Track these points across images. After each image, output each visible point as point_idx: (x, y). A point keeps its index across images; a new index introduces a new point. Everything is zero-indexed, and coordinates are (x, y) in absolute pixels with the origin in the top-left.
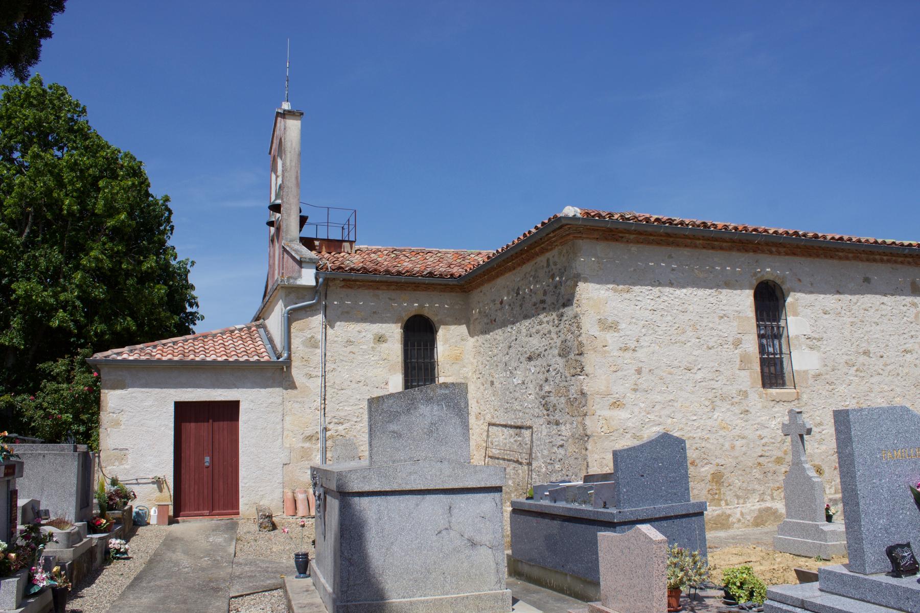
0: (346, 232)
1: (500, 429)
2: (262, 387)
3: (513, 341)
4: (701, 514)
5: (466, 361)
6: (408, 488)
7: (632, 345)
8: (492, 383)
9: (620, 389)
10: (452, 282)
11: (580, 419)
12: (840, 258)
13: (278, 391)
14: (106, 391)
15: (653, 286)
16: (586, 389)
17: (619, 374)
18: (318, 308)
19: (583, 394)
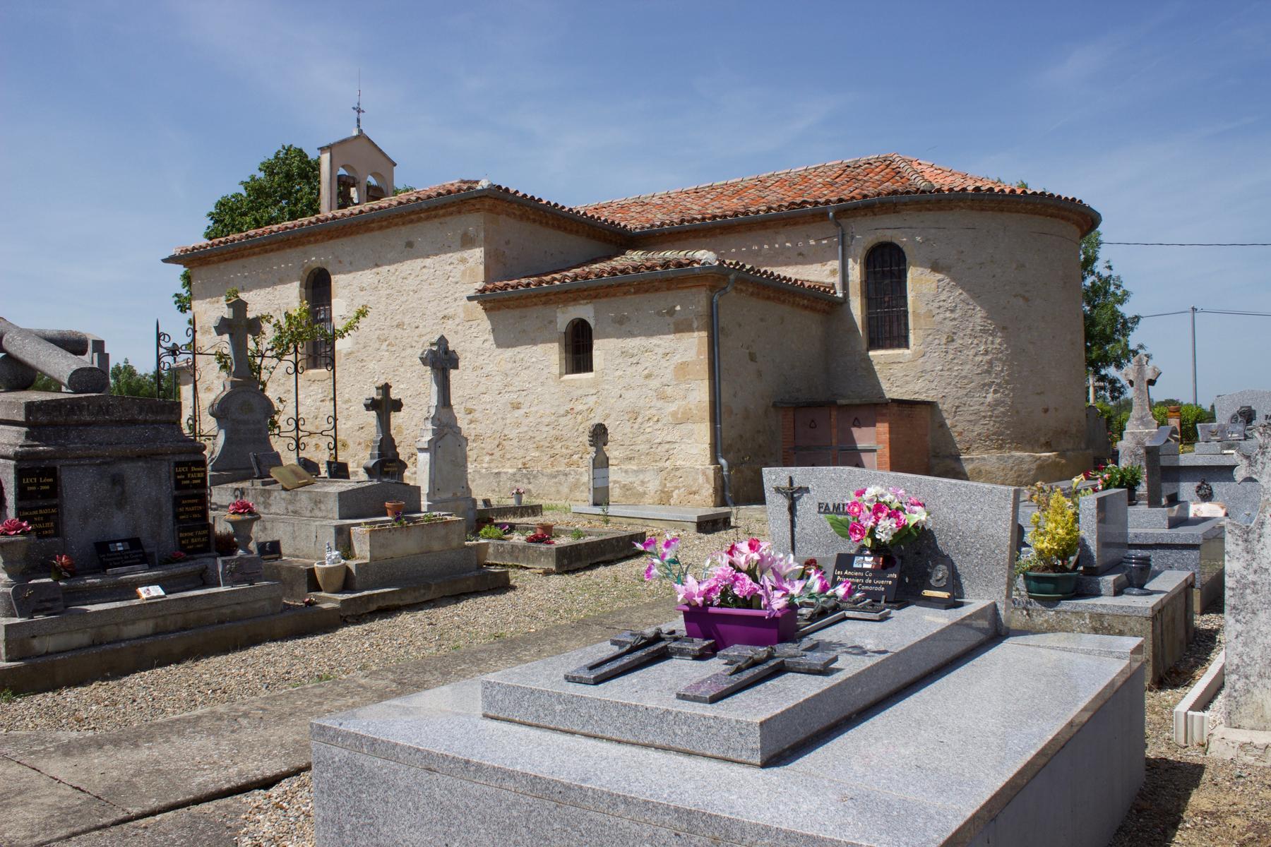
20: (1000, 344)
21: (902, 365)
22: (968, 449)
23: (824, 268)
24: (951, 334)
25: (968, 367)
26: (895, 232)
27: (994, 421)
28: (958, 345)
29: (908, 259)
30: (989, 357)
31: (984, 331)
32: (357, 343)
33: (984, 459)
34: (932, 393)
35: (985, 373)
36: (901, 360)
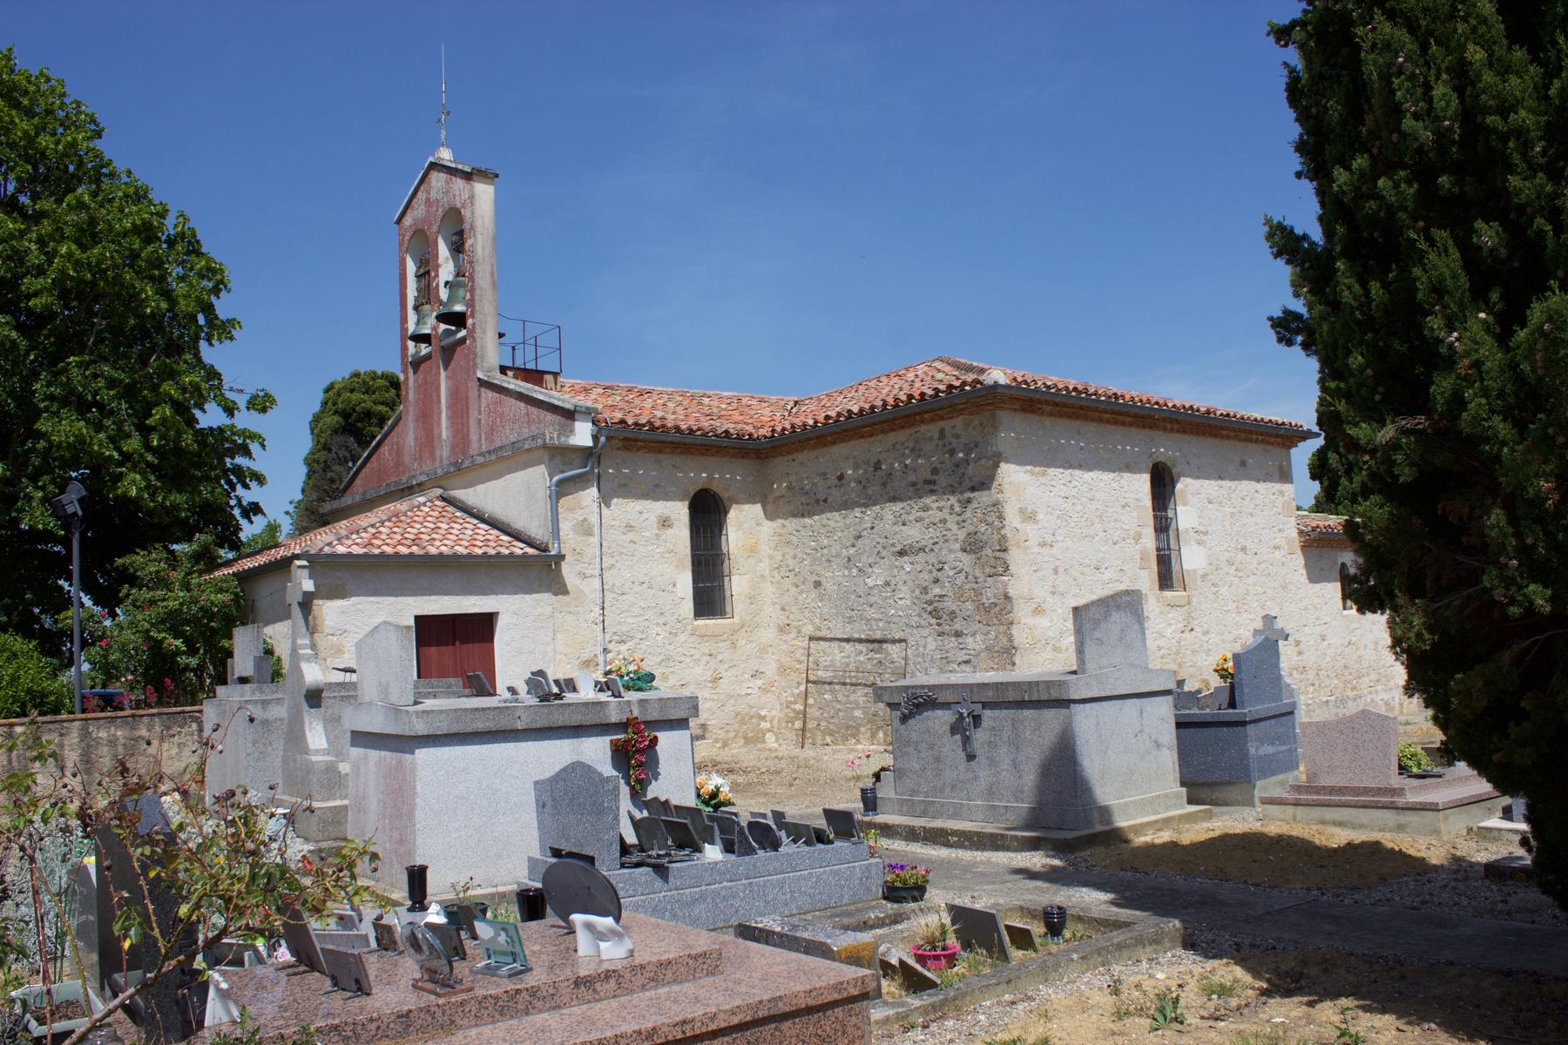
0: (519, 353)
1: (835, 644)
2: (526, 593)
3: (865, 529)
4: (1291, 713)
5: (762, 553)
6: (1116, 693)
7: (1049, 539)
8: (817, 584)
9: (1041, 592)
10: (677, 438)
11: (1002, 628)
12: (1222, 437)
13: (546, 596)
14: (321, 602)
15: (1065, 468)
16: (1011, 592)
17: (1040, 574)
18: (590, 477)
19: (1007, 597)
32: (1211, 564)
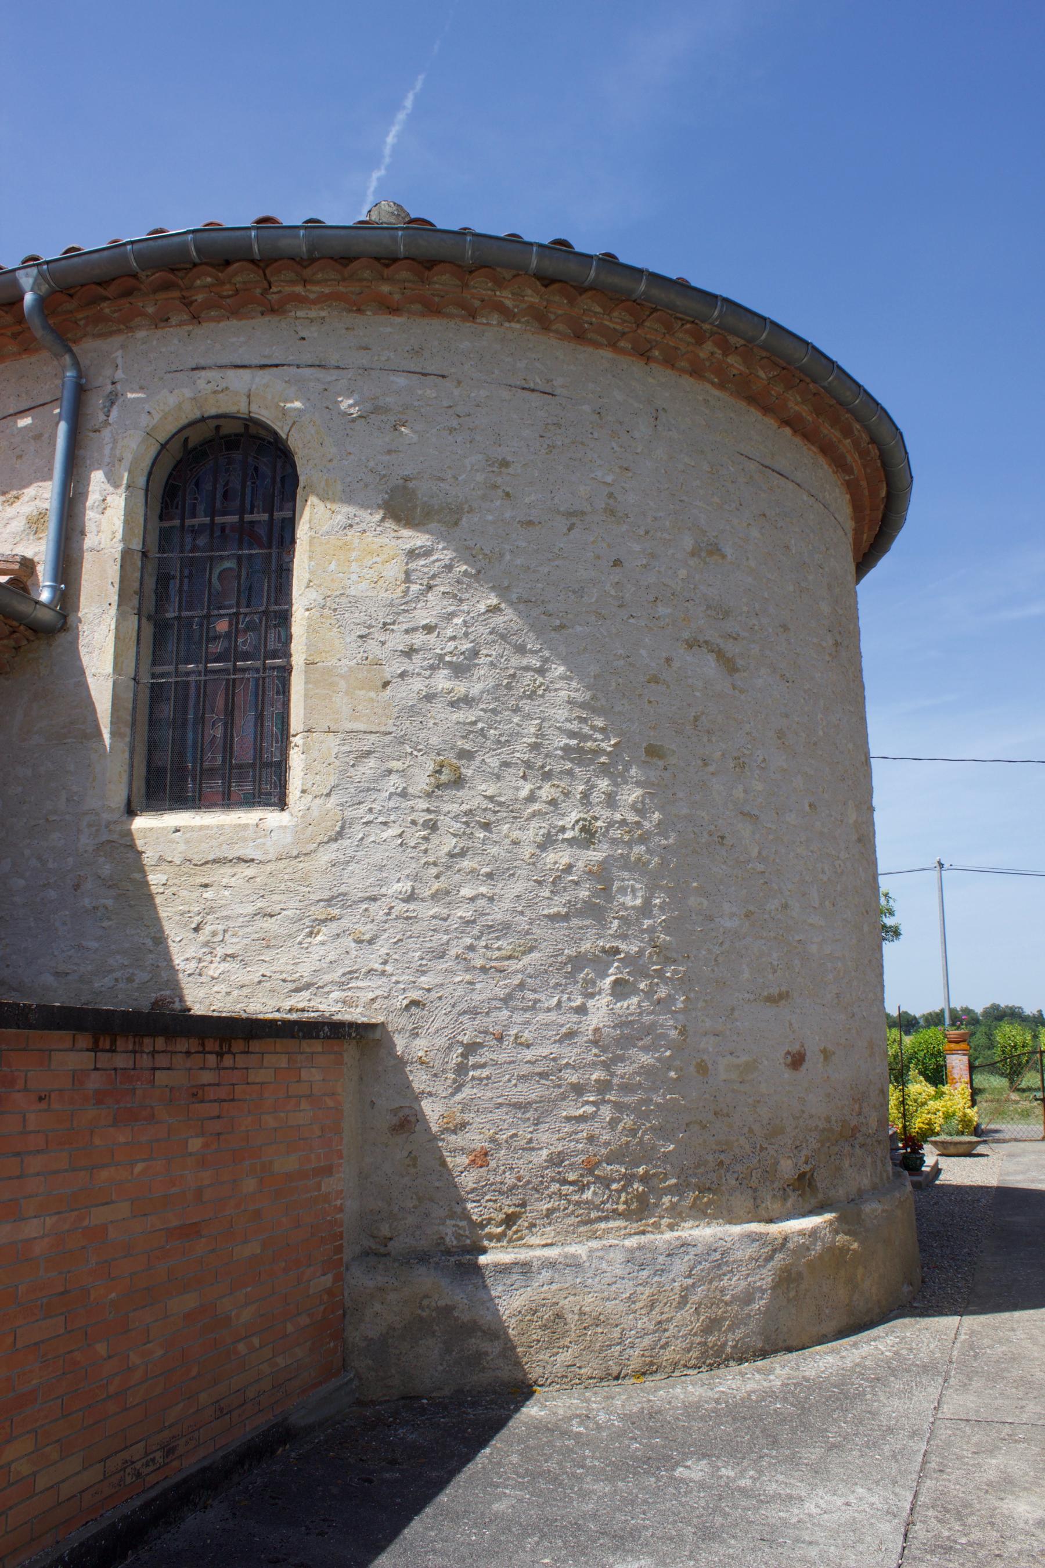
20: (640, 809)
21: (250, 871)
22: (510, 1220)
23: (10, 511)
24: (451, 757)
25: (518, 887)
26: (263, 377)
27: (618, 1106)
28: (477, 802)
29: (304, 472)
30: (596, 855)
31: (578, 755)
33: (574, 1264)
34: (367, 989)
35: (581, 914)
36: (248, 852)
